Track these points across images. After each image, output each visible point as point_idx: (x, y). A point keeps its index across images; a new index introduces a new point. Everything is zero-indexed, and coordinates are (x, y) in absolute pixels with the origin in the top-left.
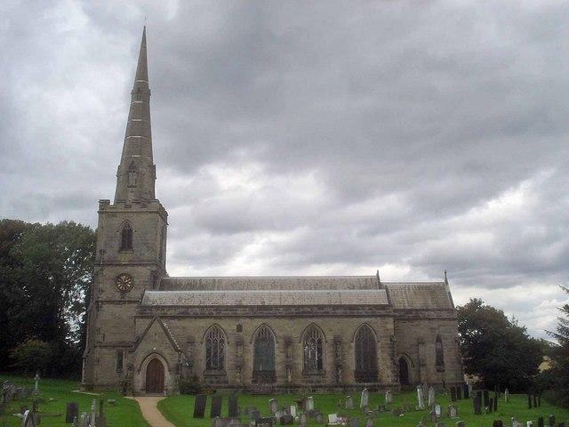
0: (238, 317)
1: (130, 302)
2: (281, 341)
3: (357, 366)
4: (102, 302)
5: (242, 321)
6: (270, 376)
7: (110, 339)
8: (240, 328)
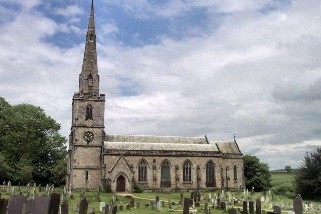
0: (154, 156)
1: (92, 146)
2: (174, 168)
3: (206, 180)
4: (77, 146)
5: (155, 158)
6: (168, 184)
7: (81, 165)
8: (154, 161)
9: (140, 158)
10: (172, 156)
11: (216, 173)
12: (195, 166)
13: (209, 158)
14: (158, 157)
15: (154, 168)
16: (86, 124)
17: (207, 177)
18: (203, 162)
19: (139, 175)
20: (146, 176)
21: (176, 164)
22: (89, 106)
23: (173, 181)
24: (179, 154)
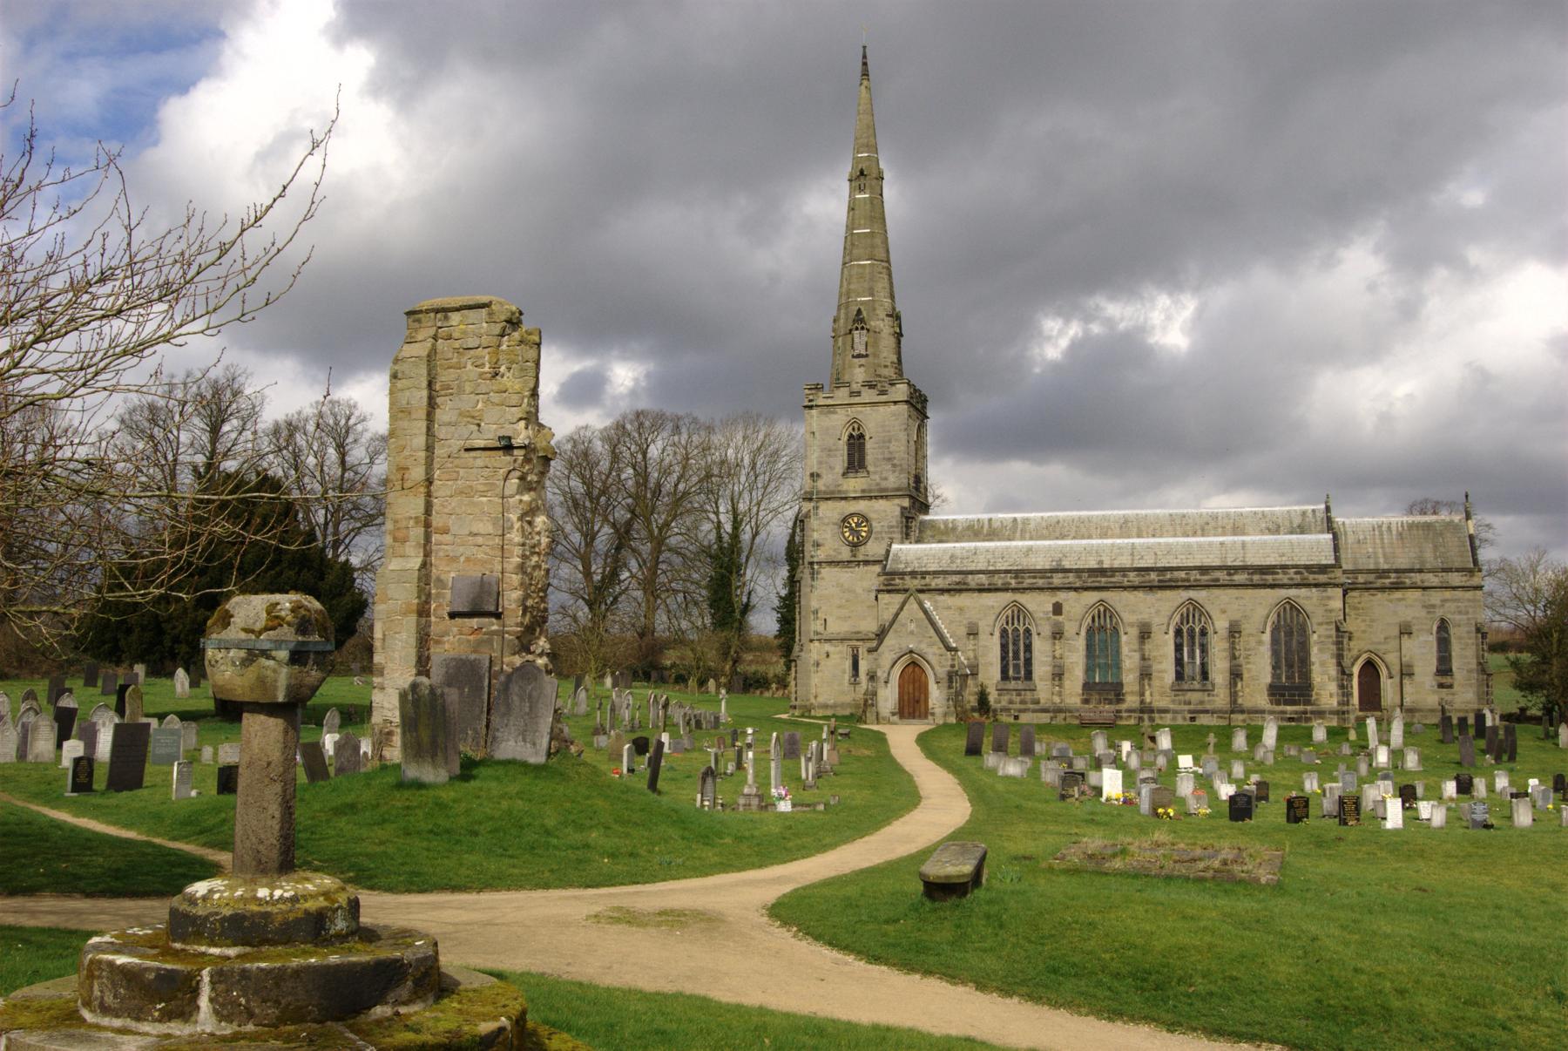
1: (867, 563)
4: (819, 563)
5: (1061, 596)
6: (1115, 691)
7: (835, 627)
8: (1058, 609)
9: (1008, 597)
10: (1125, 588)
11: (1314, 650)
12: (1221, 624)
13: (1284, 593)
14: (1072, 594)
15: (1057, 635)
16: (845, 488)
17: (1275, 667)
18: (1258, 607)
19: (1004, 658)
20: (1028, 662)
21: (1145, 617)
22: (855, 423)
23: (1129, 679)
24: (1159, 579)
